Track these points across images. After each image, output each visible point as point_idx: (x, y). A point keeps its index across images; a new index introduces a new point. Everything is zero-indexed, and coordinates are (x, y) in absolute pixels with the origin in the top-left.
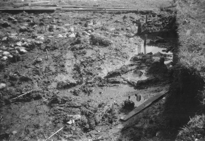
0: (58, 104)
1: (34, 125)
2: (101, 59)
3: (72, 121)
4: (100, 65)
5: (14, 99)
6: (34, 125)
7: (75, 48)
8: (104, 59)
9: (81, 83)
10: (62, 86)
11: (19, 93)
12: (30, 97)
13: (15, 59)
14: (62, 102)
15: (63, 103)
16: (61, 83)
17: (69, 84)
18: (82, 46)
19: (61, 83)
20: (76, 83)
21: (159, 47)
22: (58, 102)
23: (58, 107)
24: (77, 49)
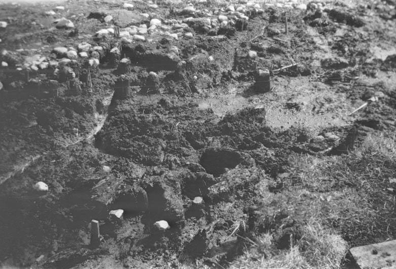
0: (340, 82)
1: (325, 99)
2: (365, 41)
3: (375, 98)
4: (392, 38)
5: (277, 71)
6: (325, 99)
7: (317, 23)
8: (369, 40)
9: (352, 65)
10: (329, 64)
11: (387, 39)
12: (296, 71)
13: (241, 27)
14: (344, 79)
15: (347, 82)
16: (328, 60)
17: (339, 63)
18: (326, 22)
19: (328, 60)
20: (347, 63)
21: (10, 4)
22: (340, 80)
23: (341, 85)
24: (319, 25)
